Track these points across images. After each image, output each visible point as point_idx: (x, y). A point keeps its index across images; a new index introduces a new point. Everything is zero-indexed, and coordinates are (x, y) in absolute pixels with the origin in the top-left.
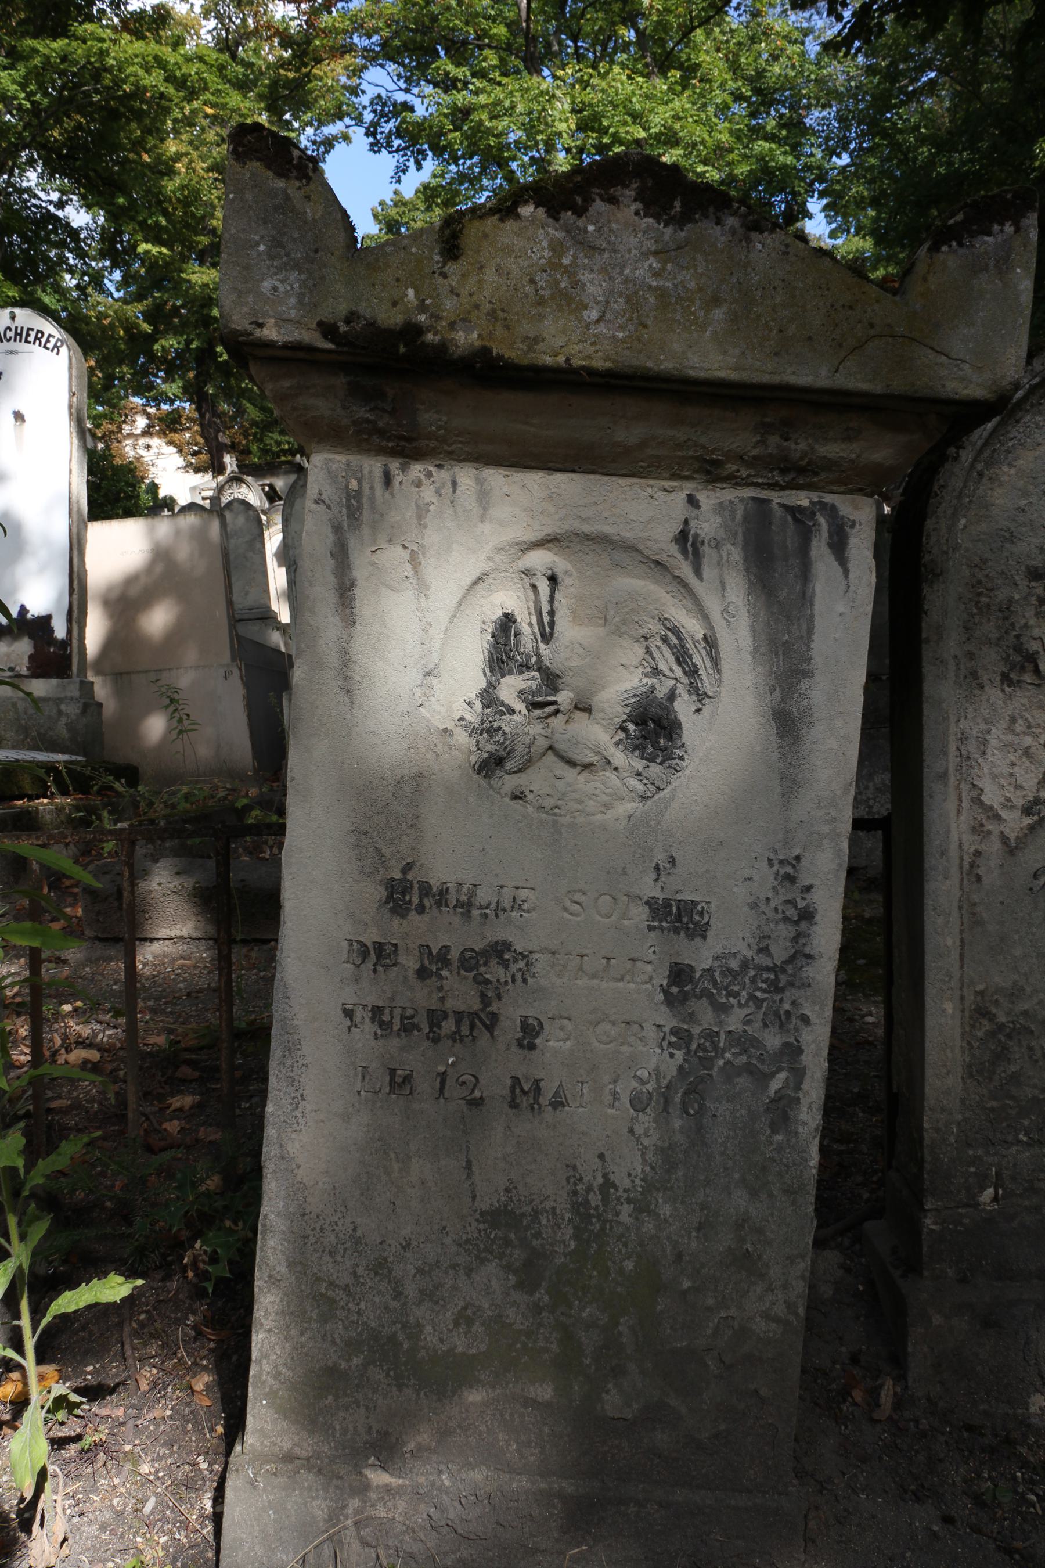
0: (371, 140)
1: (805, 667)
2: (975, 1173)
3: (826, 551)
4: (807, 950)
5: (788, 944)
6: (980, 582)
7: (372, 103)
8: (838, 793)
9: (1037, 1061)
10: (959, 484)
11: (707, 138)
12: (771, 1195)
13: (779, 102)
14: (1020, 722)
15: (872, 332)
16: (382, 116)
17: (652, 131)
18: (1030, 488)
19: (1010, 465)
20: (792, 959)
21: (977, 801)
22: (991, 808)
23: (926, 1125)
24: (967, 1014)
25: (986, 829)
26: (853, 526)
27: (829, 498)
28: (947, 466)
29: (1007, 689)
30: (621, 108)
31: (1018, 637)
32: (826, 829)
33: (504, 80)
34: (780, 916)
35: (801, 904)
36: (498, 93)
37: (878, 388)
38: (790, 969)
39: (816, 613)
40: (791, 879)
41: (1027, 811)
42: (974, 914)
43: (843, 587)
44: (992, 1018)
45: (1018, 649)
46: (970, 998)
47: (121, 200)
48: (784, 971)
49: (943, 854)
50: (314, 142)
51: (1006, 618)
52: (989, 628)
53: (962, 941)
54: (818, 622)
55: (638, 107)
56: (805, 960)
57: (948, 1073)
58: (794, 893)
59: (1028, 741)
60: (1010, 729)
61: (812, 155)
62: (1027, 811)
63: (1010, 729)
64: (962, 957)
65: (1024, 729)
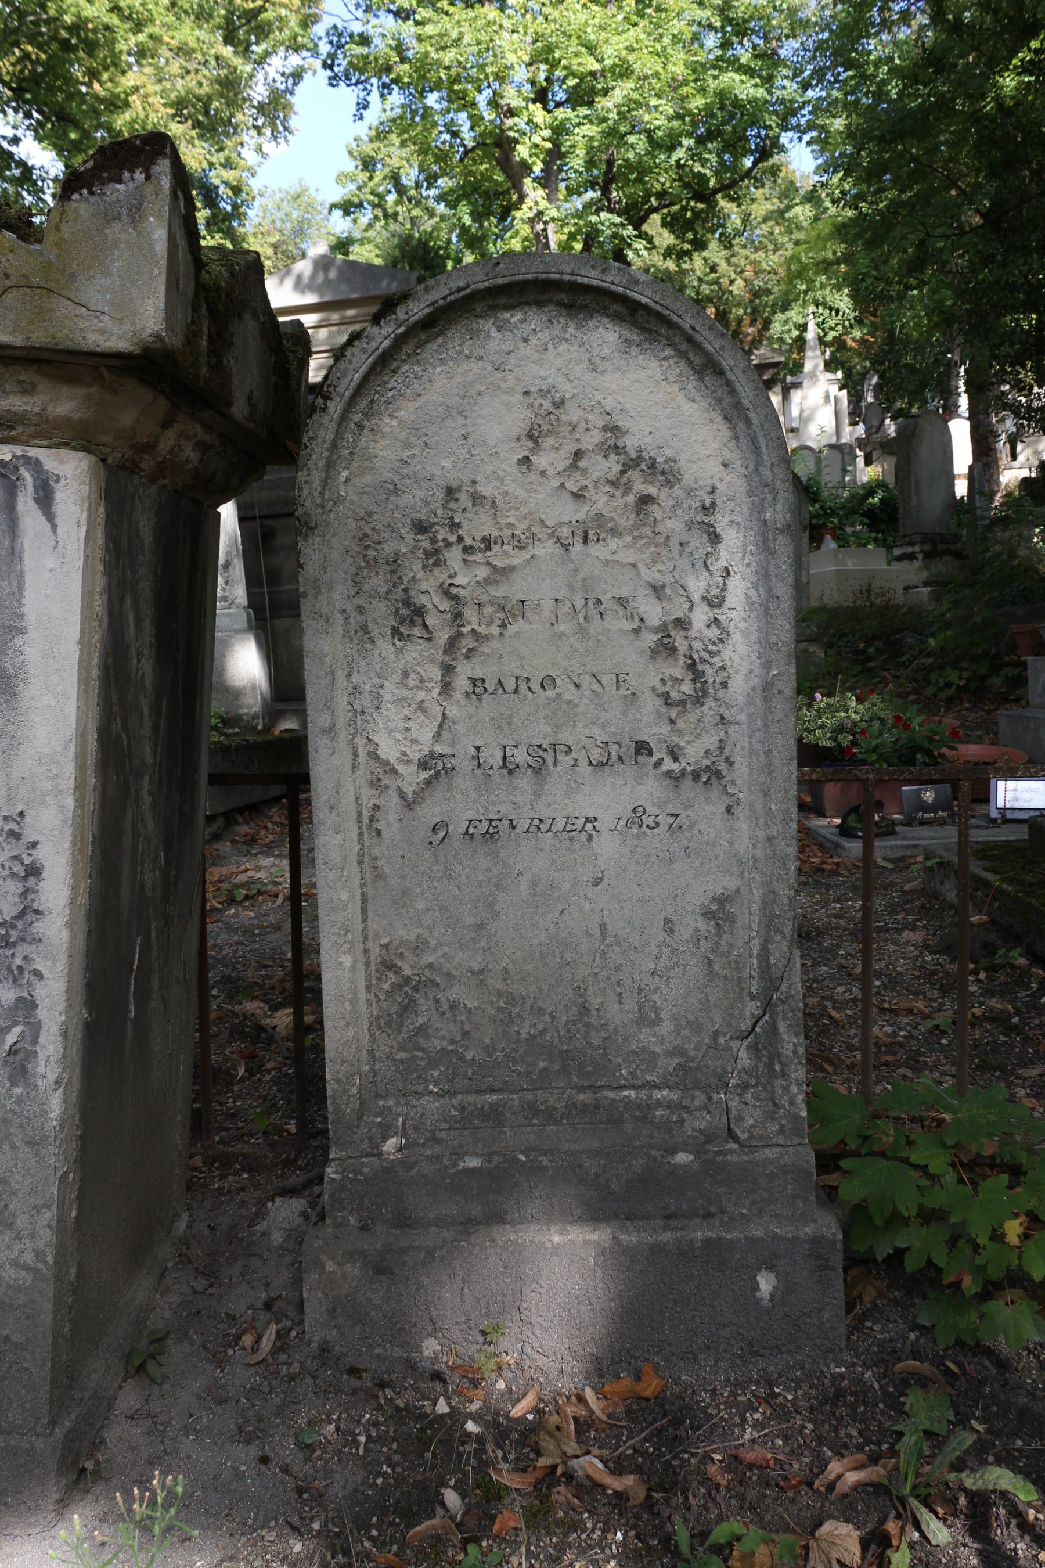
0: (329, 73)
1: (18, 623)
2: (380, 1124)
3: (32, 506)
4: (35, 906)
5: (17, 900)
6: (366, 535)
7: (328, 34)
8: (59, 749)
9: (443, 1013)
10: (330, 436)
11: (661, 71)
12: (13, 1147)
13: (753, 31)
14: (413, 676)
15: (8, 283)
16: (339, 48)
17: (606, 62)
18: (413, 439)
19: (391, 416)
20: (22, 914)
21: (374, 755)
22: (388, 763)
23: (328, 1077)
24: (373, 967)
25: (383, 783)
26: (57, 481)
27: (33, 452)
28: (315, 417)
29: (398, 643)
30: (574, 38)
31: (406, 590)
32: (48, 785)
33: (451, 9)
34: (7, 872)
35: (27, 860)
36: (445, 22)
37: (18, 340)
38: (20, 924)
39: (26, 568)
40: (16, 836)
41: (423, 765)
42: (375, 868)
43: (53, 543)
44: (398, 971)
45: (407, 603)
46: (375, 952)
47: (73, 136)
48: (14, 926)
49: (331, 808)
50: (283, 74)
51: (393, 572)
52: (378, 582)
53: (363, 894)
54: (29, 578)
55: (592, 37)
56: (34, 916)
57: (348, 1025)
58: (20, 849)
59: (421, 695)
60: (403, 683)
61: (784, 88)
62: (423, 765)
63: (403, 683)
64: (364, 911)
65: (417, 682)
